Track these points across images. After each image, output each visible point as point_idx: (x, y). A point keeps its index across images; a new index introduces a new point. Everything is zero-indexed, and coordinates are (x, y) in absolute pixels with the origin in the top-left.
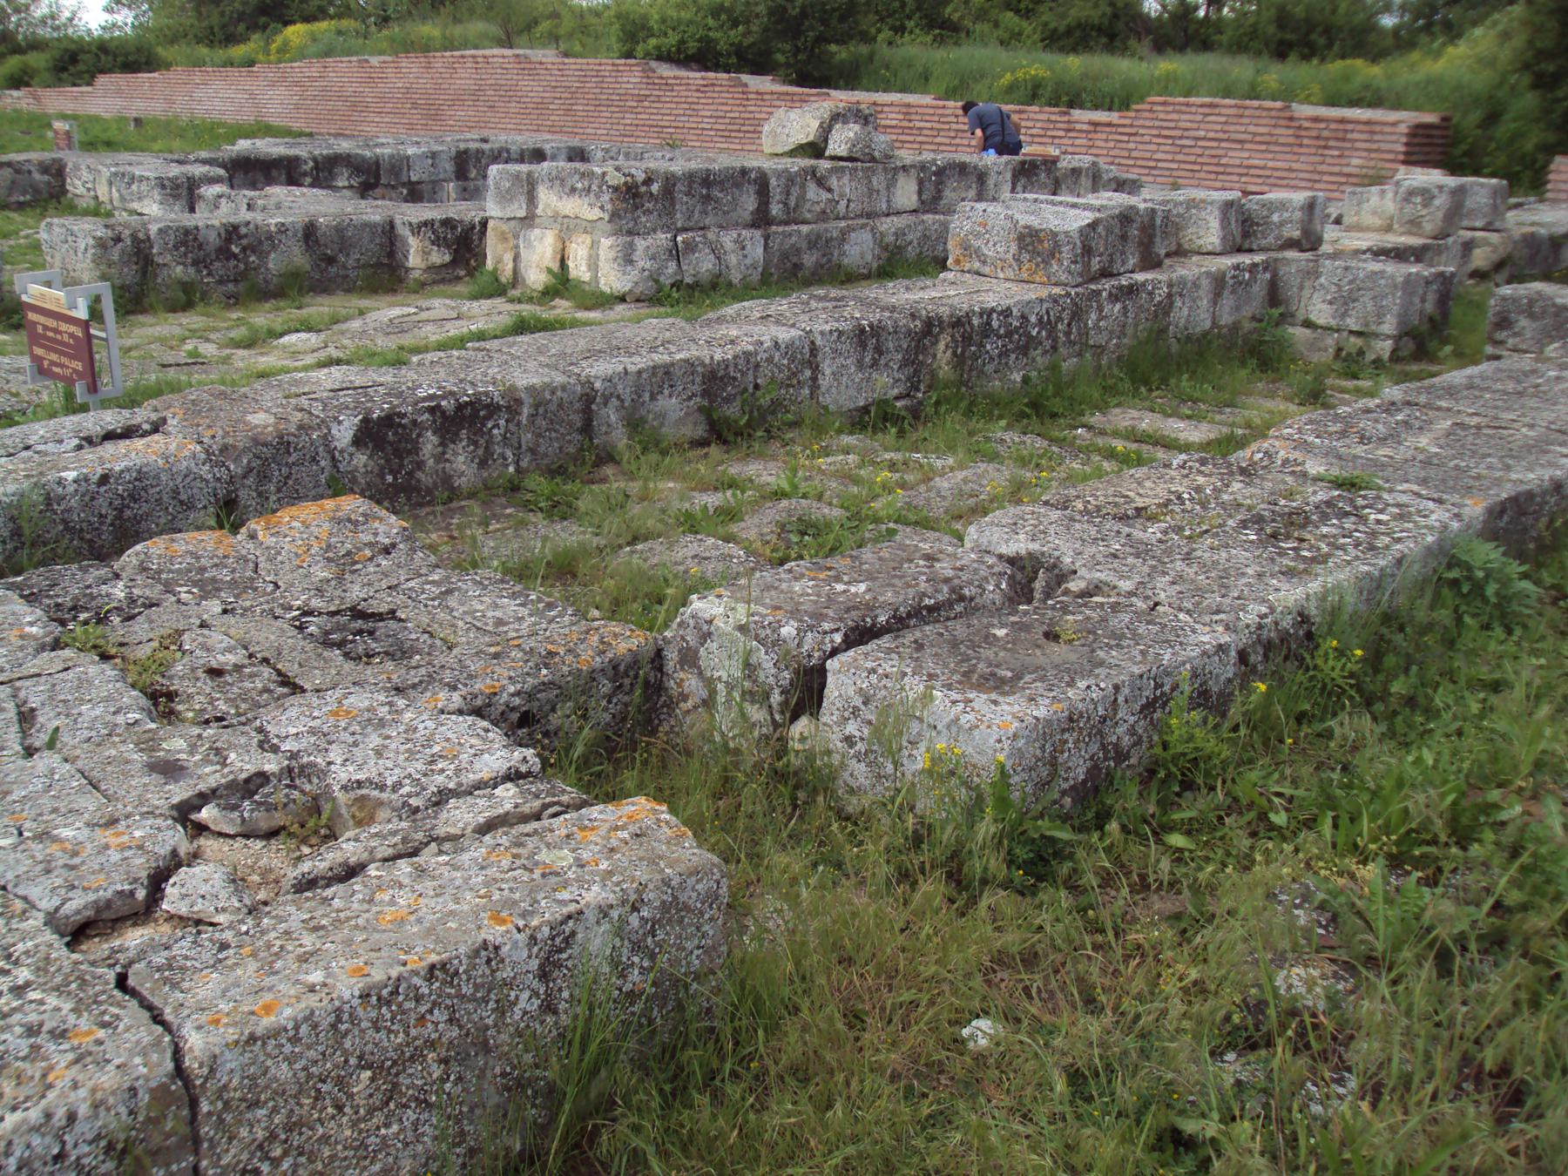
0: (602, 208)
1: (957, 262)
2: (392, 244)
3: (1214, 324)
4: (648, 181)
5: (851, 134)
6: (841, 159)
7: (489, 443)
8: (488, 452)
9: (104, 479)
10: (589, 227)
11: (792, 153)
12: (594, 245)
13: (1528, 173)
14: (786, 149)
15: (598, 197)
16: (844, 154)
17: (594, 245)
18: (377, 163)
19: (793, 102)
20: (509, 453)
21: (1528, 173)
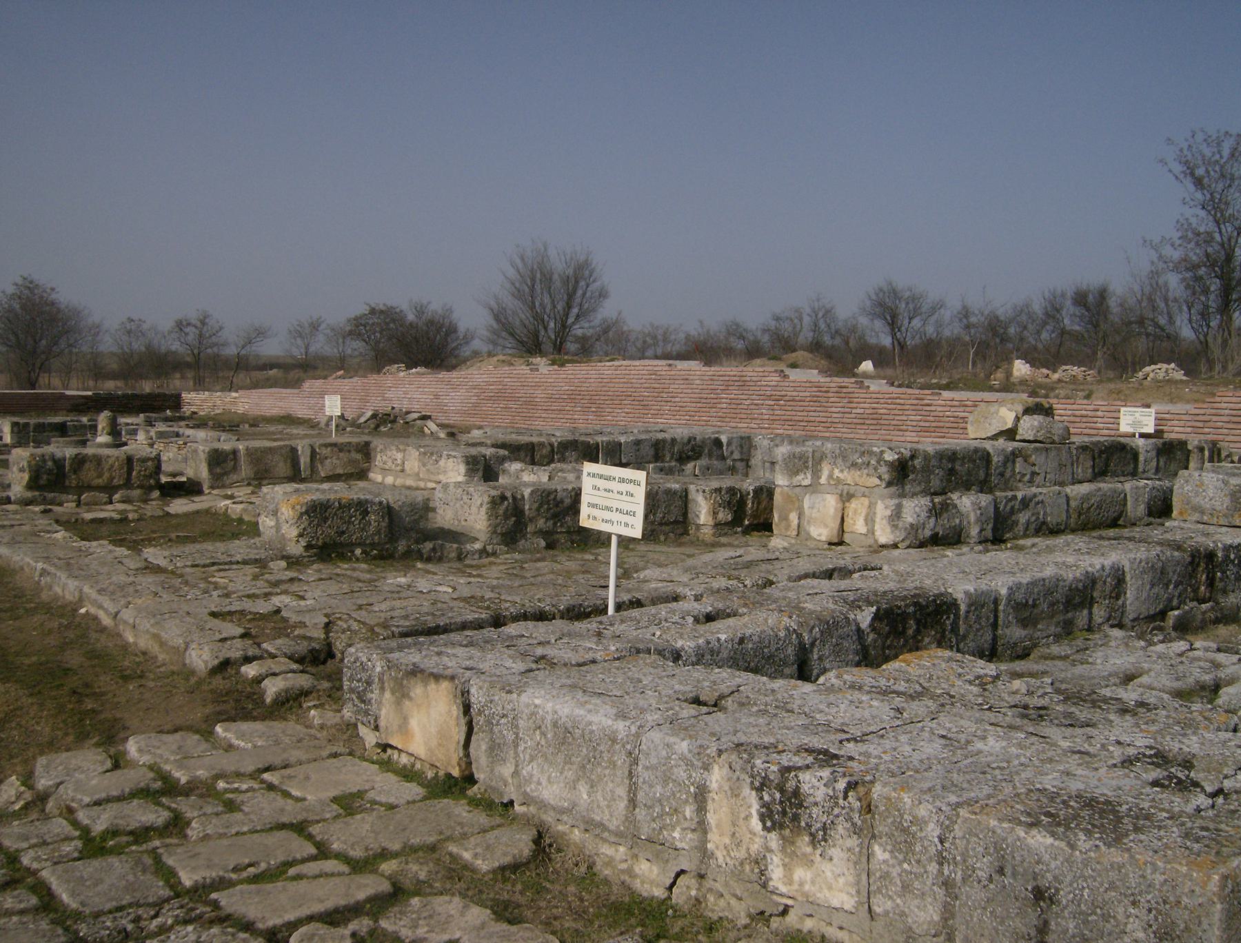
0: (880, 478)
1: (1181, 513)
2: (686, 506)
3: (466, 907)
4: (913, 457)
5: (1036, 423)
6: (1029, 441)
7: (944, 631)
8: (943, 636)
9: (742, 641)
10: (868, 492)
11: (994, 437)
12: (871, 506)
13: (967, 338)
14: (989, 435)
15: (876, 469)
16: (1031, 438)
17: (871, 506)
18: (598, 444)
19: (1001, 403)
20: (954, 640)
21: (967, 338)
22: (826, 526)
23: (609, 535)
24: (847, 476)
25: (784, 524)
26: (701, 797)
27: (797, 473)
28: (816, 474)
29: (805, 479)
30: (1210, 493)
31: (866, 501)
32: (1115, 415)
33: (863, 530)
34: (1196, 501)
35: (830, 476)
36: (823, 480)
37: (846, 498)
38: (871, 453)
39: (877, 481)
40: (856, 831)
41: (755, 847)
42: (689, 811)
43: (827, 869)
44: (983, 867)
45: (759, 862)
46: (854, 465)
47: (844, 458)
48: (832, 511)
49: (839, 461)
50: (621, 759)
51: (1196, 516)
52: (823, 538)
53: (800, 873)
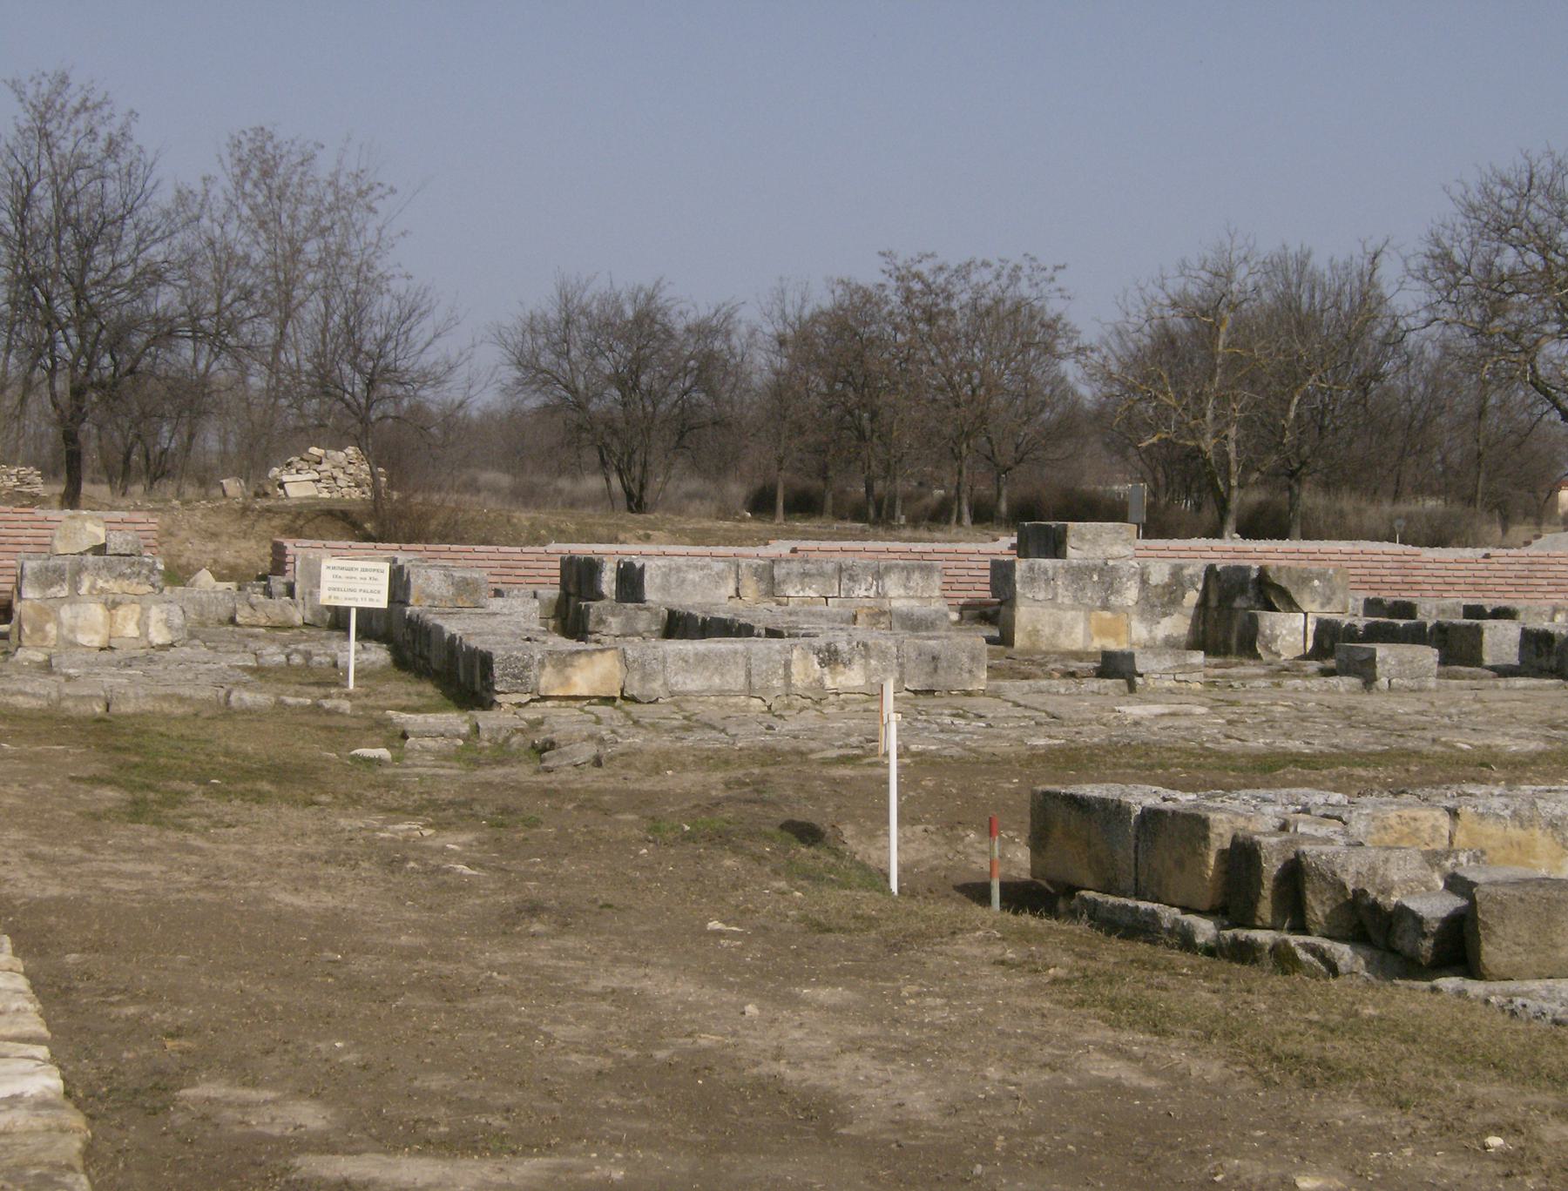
0: (153, 585)
12: (145, 611)
15: (148, 578)
22: (97, 632)
23: (348, 609)
24: (114, 586)
25: (37, 637)
26: (787, 665)
27: (51, 585)
28: (75, 586)
29: (63, 591)
30: (437, 583)
31: (137, 608)
32: (47, 540)
33: (136, 634)
34: (429, 590)
35: (93, 587)
36: (84, 590)
37: (113, 606)
38: (142, 564)
39: (150, 589)
40: (863, 657)
41: (817, 675)
42: (781, 671)
43: (852, 674)
44: (913, 655)
45: (820, 681)
46: (122, 575)
47: (110, 570)
48: (101, 618)
49: (104, 572)
50: (741, 660)
51: (429, 602)
52: (96, 644)
53: (840, 678)
